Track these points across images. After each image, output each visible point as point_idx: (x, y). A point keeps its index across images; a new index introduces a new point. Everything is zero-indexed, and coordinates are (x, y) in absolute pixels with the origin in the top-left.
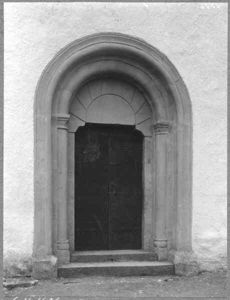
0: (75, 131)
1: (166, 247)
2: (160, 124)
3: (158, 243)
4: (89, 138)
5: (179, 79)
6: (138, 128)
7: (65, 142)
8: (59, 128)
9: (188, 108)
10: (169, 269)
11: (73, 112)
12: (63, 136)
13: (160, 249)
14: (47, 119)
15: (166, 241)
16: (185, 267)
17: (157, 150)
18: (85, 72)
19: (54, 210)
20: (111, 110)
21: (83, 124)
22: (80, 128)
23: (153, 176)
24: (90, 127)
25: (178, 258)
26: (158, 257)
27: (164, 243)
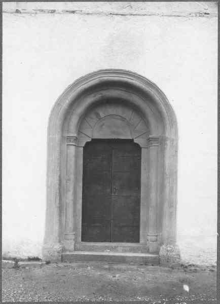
0: (83, 145)
1: (156, 240)
2: (152, 138)
3: (149, 238)
4: (94, 151)
5: (167, 105)
6: (136, 141)
7: (73, 153)
8: (67, 145)
9: (174, 123)
10: (123, 283)
11: (81, 130)
12: (72, 150)
13: (150, 242)
14: (57, 137)
15: (157, 236)
16: (168, 260)
17: (149, 155)
18: (90, 100)
19: (61, 209)
20: (110, 126)
21: (89, 140)
22: (87, 143)
23: (148, 176)
24: (95, 141)
25: (162, 252)
26: (149, 249)
27: (156, 237)
